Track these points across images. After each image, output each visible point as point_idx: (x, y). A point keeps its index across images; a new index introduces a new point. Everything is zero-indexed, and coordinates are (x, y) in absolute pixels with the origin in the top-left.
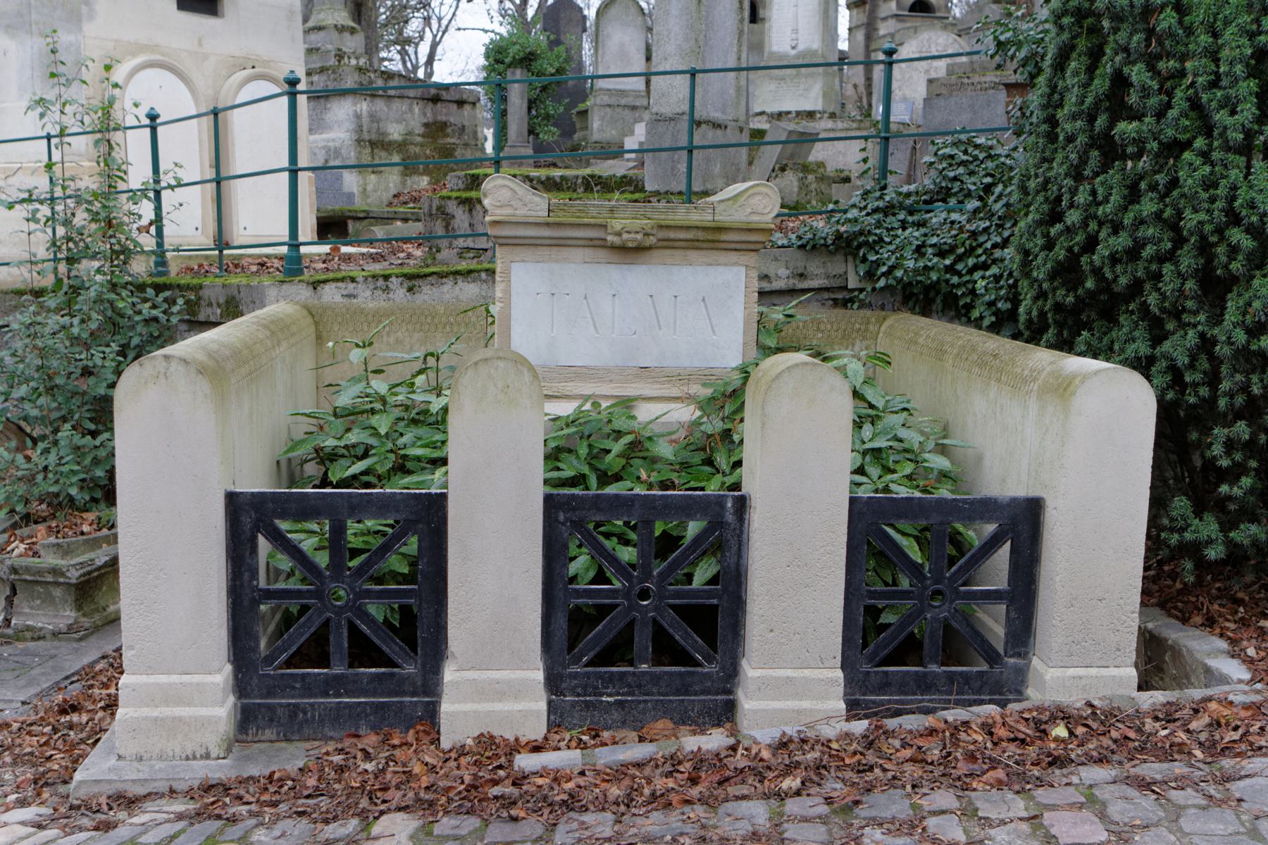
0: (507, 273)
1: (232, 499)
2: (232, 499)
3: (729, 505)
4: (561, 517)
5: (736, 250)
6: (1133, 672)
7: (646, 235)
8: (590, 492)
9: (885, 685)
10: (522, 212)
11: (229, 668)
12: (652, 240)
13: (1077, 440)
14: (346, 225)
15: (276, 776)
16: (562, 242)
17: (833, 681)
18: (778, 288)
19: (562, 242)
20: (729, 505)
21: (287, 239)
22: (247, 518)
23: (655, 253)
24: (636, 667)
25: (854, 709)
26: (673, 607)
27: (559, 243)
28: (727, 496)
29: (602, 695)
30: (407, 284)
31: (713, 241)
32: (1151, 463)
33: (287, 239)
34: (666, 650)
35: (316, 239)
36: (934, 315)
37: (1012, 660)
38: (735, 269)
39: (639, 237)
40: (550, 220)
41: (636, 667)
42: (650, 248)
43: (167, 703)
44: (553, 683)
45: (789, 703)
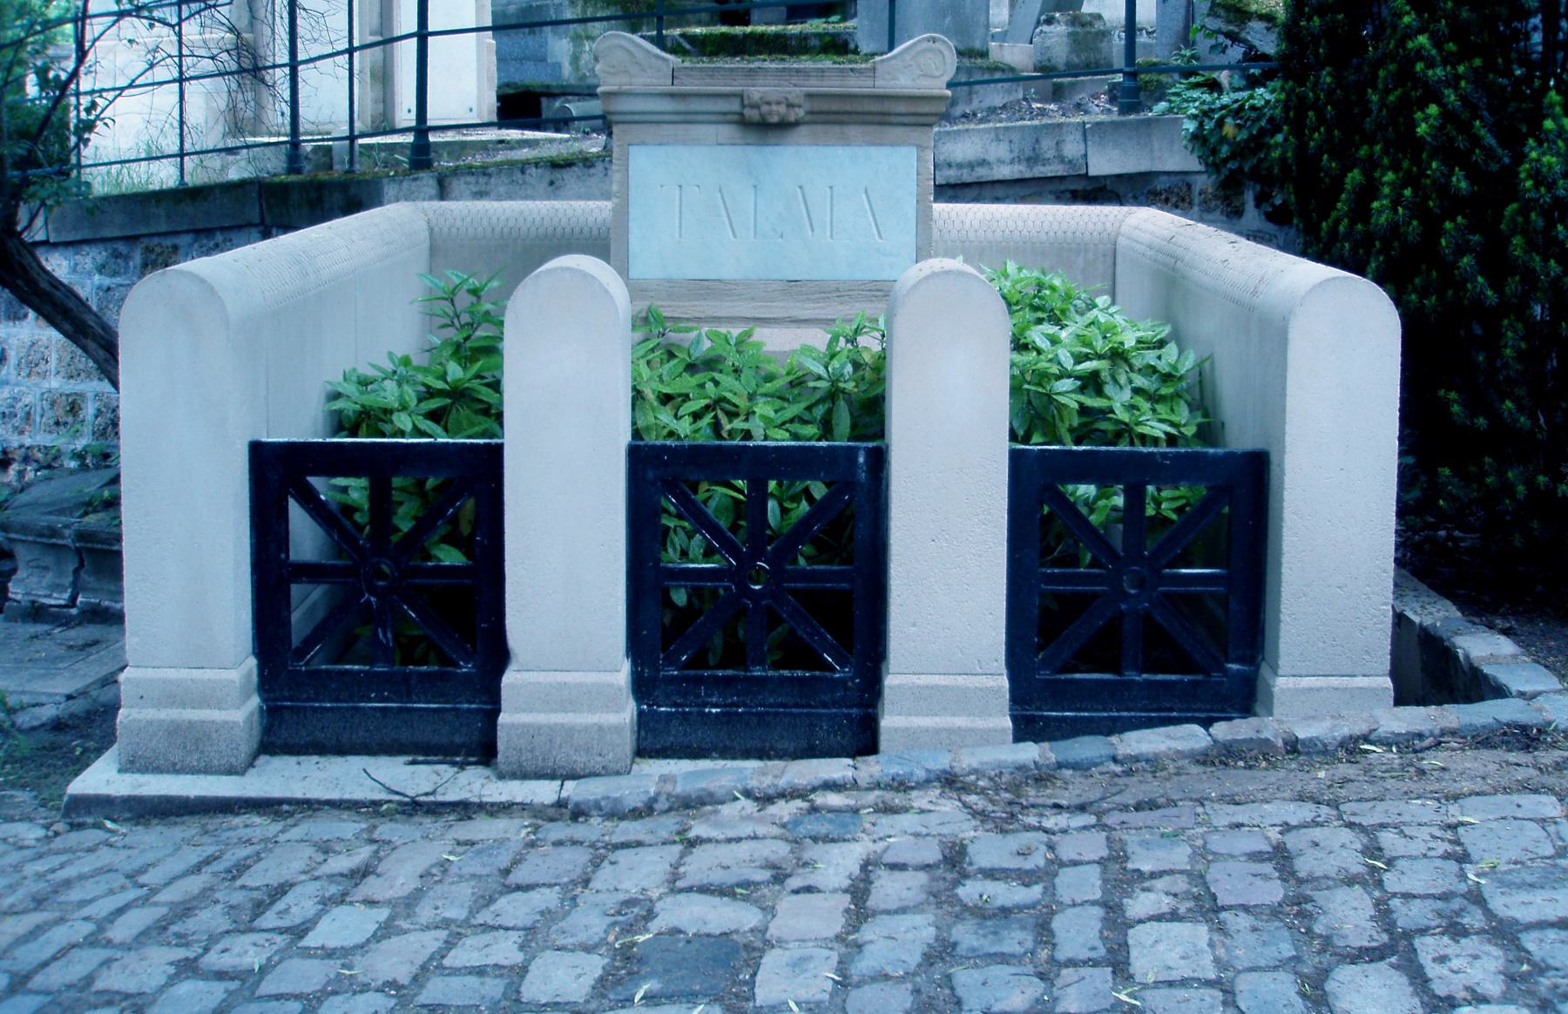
0: (626, 157)
1: (258, 451)
2: (258, 451)
3: (861, 460)
4: (650, 475)
5: (904, 125)
6: (1387, 682)
7: (790, 106)
8: (750, 444)
9: (1061, 694)
10: (640, 82)
11: (253, 662)
12: (801, 113)
13: (1328, 374)
14: (539, 104)
15: (1309, 907)
16: (690, 117)
17: (995, 691)
18: (1000, 177)
19: (690, 117)
20: (861, 460)
21: (413, 124)
22: (277, 473)
23: (803, 130)
24: (747, 669)
25: (1026, 729)
26: (792, 591)
27: (687, 119)
28: (854, 450)
29: (705, 705)
30: (548, 175)
31: (883, 114)
32: (1398, 406)
33: (413, 124)
34: (797, 654)
35: (495, 119)
36: (390, 190)
37: (1234, 666)
38: (904, 150)
39: (782, 109)
40: (675, 89)
41: (747, 669)
42: (797, 124)
43: (183, 705)
44: (642, 687)
45: (937, 719)
